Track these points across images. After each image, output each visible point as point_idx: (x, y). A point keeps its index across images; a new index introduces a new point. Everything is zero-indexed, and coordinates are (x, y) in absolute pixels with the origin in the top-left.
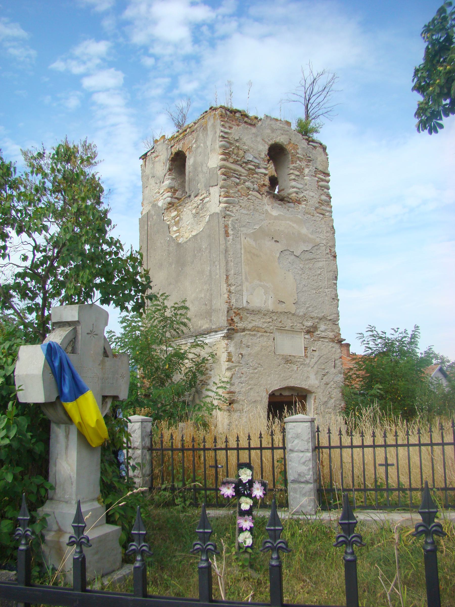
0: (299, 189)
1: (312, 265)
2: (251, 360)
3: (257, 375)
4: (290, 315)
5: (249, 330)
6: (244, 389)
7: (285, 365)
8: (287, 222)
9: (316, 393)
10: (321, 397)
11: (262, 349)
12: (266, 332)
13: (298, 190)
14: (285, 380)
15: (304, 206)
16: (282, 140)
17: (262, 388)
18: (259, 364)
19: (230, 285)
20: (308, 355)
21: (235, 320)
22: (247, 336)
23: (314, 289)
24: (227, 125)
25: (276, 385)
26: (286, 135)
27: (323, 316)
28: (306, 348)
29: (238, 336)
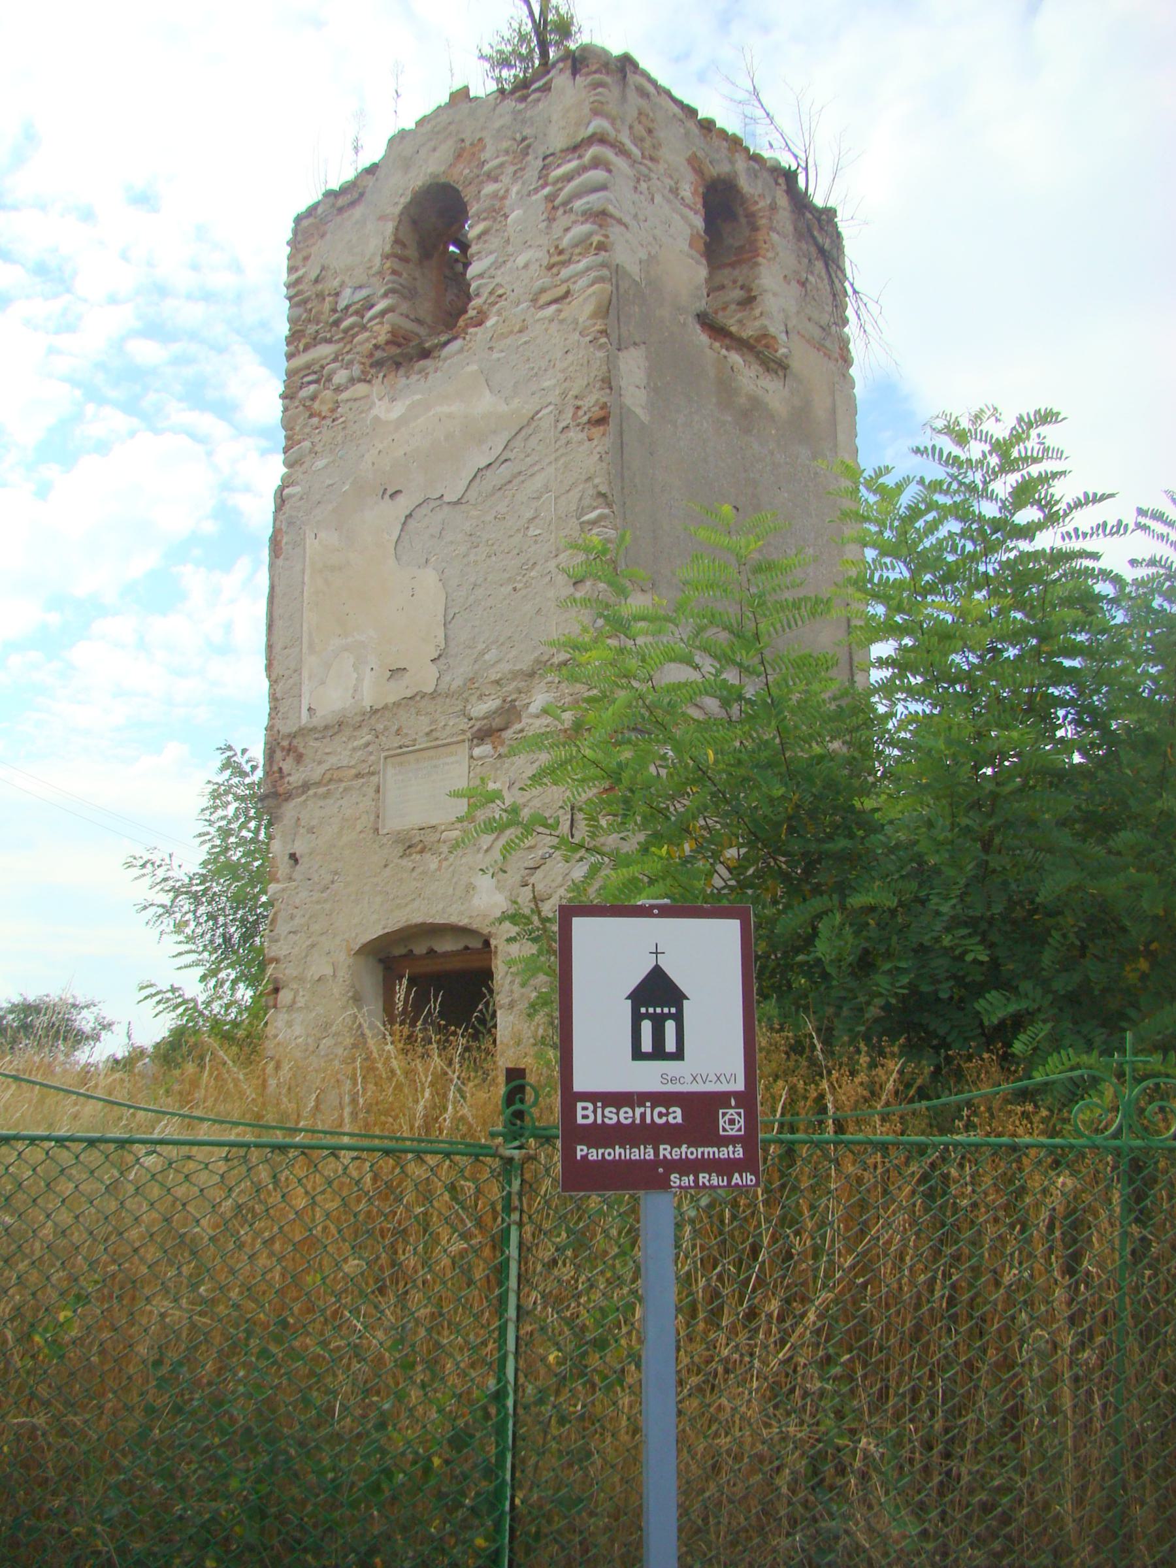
4: (423, 703)
5: (318, 784)
12: (358, 776)
18: (336, 873)
27: (537, 661)
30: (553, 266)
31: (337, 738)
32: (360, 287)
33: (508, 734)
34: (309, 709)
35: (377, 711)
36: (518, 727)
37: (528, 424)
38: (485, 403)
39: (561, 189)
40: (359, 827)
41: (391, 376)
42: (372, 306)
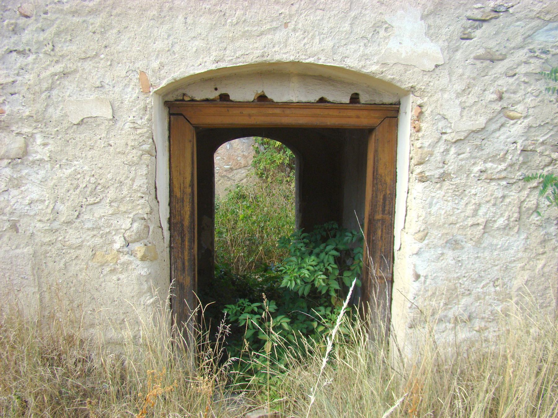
6: (30, 77)
14: (247, 35)
17: (120, 71)
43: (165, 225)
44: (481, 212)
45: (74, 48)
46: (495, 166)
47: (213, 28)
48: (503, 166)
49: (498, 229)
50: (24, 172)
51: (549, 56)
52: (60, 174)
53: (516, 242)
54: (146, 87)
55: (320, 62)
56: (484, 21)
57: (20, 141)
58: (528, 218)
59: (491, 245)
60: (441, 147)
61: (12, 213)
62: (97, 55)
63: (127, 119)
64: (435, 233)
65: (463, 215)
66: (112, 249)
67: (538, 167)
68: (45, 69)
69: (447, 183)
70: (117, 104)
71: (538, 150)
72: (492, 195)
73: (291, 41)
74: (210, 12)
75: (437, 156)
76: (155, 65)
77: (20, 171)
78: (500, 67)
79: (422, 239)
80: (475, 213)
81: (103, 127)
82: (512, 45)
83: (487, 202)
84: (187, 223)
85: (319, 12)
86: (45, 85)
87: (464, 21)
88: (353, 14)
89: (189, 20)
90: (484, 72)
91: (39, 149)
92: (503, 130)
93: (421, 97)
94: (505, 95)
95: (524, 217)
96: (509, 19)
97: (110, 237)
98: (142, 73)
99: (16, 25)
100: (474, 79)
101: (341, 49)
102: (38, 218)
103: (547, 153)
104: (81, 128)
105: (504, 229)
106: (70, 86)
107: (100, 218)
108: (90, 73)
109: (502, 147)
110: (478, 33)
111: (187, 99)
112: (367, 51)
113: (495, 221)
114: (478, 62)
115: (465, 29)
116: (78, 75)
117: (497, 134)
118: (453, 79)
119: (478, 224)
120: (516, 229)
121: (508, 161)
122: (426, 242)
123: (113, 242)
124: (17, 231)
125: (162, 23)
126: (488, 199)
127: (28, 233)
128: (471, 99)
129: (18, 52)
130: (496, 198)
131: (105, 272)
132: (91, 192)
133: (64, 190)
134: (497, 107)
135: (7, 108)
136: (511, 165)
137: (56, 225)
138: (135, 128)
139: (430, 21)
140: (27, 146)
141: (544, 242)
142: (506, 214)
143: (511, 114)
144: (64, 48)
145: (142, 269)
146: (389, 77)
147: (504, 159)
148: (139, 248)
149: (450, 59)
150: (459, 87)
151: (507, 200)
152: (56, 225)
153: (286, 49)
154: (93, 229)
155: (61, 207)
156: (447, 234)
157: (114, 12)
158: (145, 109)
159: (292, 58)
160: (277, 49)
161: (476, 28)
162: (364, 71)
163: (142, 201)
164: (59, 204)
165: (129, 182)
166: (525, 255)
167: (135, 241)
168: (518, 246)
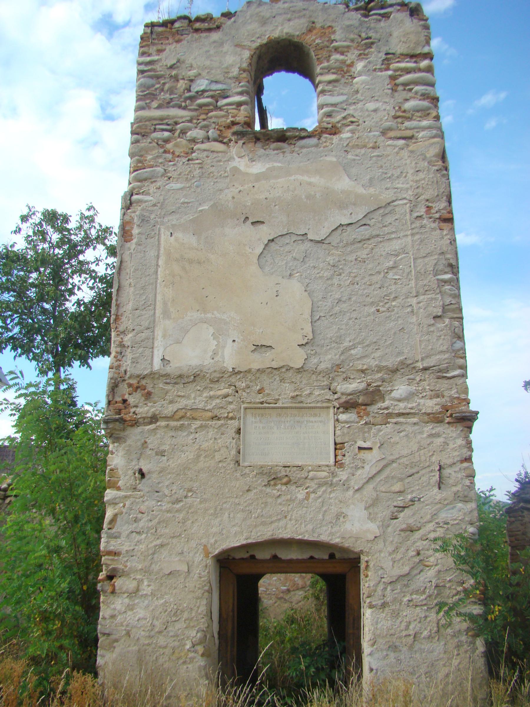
0: (333, 105)
1: (366, 252)
2: (167, 483)
3: (181, 516)
4: (290, 374)
6: (142, 547)
7: (268, 490)
8: (293, 178)
9: (368, 554)
10: (387, 564)
11: (199, 456)
12: (215, 418)
13: (330, 109)
14: (263, 524)
15: (349, 135)
16: (285, 31)
17: (193, 544)
18: (190, 490)
19: (123, 332)
20: (347, 460)
21: (131, 400)
22: (160, 432)
23: (372, 303)
24: (153, 50)
25: (235, 533)
26: (299, 18)
27: (402, 363)
28: (338, 446)
29: (135, 435)
30: (399, 117)
31: (190, 386)
32: (216, 82)
33: (373, 409)
34: (163, 359)
35: (239, 372)
36: (380, 405)
37: (385, 207)
38: (343, 183)
39: (401, 76)
40: (218, 456)
41: (251, 145)
42: (227, 97)
43: (216, 636)
44: (411, 627)
45: (167, 531)
46: (418, 597)
47: (244, 519)
48: (423, 597)
49: (424, 638)
50: (136, 601)
51: (449, 526)
52: (156, 603)
53: (438, 647)
54: (207, 554)
55: (306, 538)
56: (404, 507)
57: (134, 584)
58: (445, 630)
59: (421, 649)
60: (381, 586)
61: (127, 626)
62: (180, 535)
63: (196, 571)
64: (380, 640)
65: (399, 629)
66: (184, 649)
67: (448, 597)
68: (151, 542)
69: (387, 609)
70: (190, 563)
71: (447, 585)
72: (417, 616)
73: (288, 526)
74: (243, 511)
75: (379, 592)
76: (212, 541)
77: (134, 600)
78: (417, 535)
79: (373, 645)
80: (407, 628)
81: (182, 576)
82: (425, 521)
83: (415, 620)
84: (229, 634)
85: (304, 509)
86: (151, 552)
87: (392, 508)
88: (324, 509)
89: (231, 516)
90: (407, 539)
91: (146, 588)
92: (422, 574)
93: (367, 556)
94: (422, 552)
95: (442, 630)
96: (421, 505)
97: (183, 641)
98: (205, 546)
99: (136, 518)
100: (400, 543)
101: (317, 530)
102: (142, 629)
103: (454, 587)
104: (170, 576)
105: (429, 638)
106: (164, 553)
107: (179, 630)
108: (176, 545)
109: (422, 585)
110: (402, 515)
111: (231, 558)
112: (333, 530)
113: (421, 633)
114: (402, 533)
115: (393, 513)
116: (169, 546)
117: (418, 577)
118: (387, 544)
119: (410, 635)
120: (437, 638)
121: (427, 594)
122: (375, 647)
123: (185, 644)
124: (130, 636)
125: (216, 517)
126: (415, 618)
127: (136, 638)
128: (399, 556)
129: (137, 533)
130: (420, 618)
131: (179, 663)
132: (174, 614)
133: (158, 612)
134: (417, 560)
135: (129, 564)
136: (430, 596)
137: (153, 633)
138: (200, 577)
139: (371, 510)
140: (138, 586)
141: (458, 646)
142: (429, 628)
143: (427, 563)
144: (162, 530)
145: (201, 662)
146: (346, 545)
147: (424, 592)
148: (200, 649)
149: (384, 532)
150: (390, 549)
151: (429, 619)
152: (153, 633)
153: (286, 532)
154: (174, 636)
155: (156, 623)
156: (389, 642)
157: (190, 511)
158: (206, 566)
159: (289, 536)
160: (280, 531)
161: (401, 512)
162: (332, 542)
163: (203, 620)
164: (155, 620)
165: (196, 608)
166: (445, 656)
167: (197, 644)
168: (439, 650)
